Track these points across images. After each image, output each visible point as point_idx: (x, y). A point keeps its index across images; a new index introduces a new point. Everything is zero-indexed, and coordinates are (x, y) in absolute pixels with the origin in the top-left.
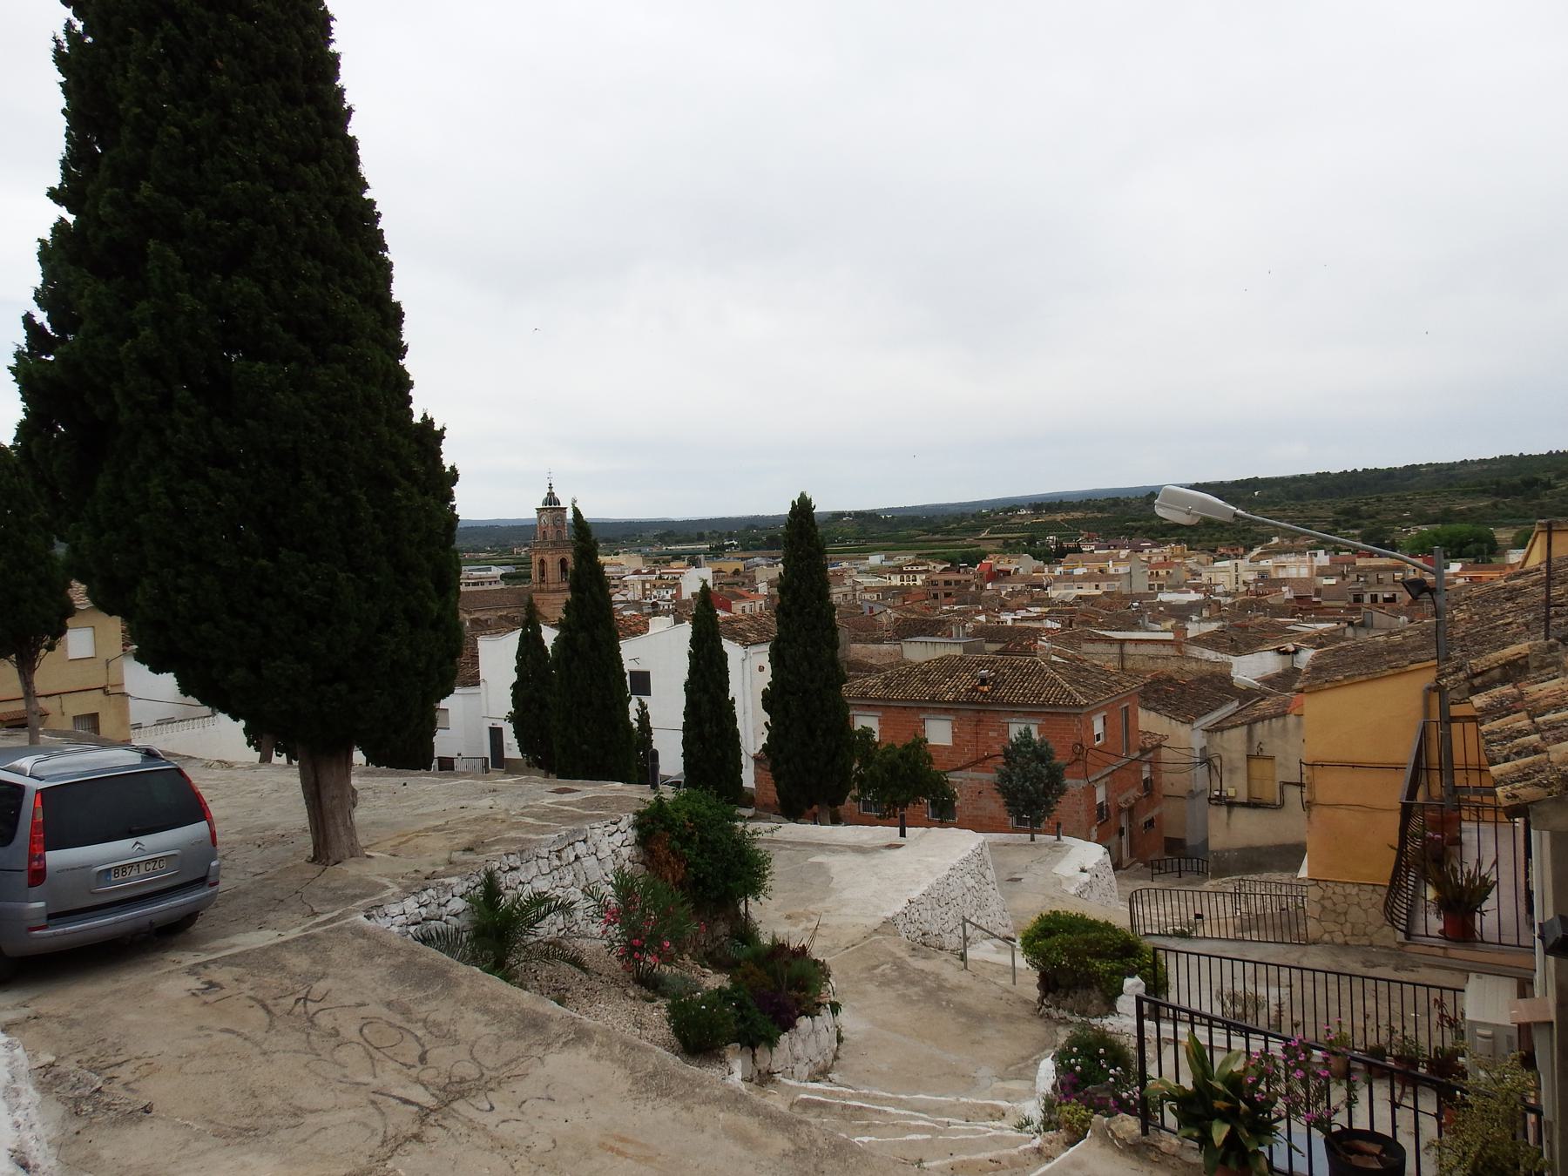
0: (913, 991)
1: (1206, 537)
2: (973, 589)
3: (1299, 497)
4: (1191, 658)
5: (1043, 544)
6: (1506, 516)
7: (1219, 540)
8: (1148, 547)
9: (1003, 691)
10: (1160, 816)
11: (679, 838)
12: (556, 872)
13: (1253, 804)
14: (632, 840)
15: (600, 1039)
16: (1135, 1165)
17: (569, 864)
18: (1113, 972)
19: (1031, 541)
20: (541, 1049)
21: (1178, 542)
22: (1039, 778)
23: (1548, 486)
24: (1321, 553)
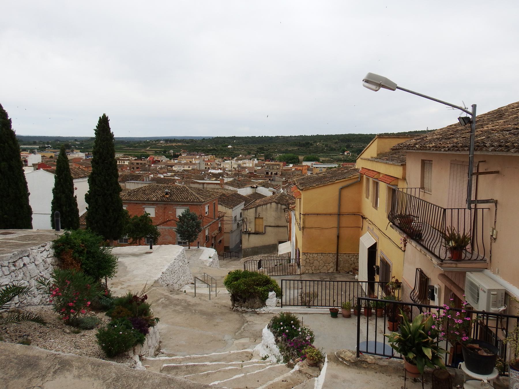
0: (178, 308)
1: (221, 154)
2: (147, 166)
3: (247, 143)
4: (225, 189)
5: (169, 153)
6: (301, 152)
7: (224, 155)
8: (203, 156)
9: (174, 197)
10: (223, 239)
11: (77, 251)
12: (13, 273)
13: (256, 233)
14: (52, 255)
15: (77, 364)
16: (358, 371)
17: (20, 268)
18: (265, 291)
19: (165, 152)
20: (39, 380)
21: (212, 155)
22: (193, 227)
23: (312, 145)
24: (256, 159)
